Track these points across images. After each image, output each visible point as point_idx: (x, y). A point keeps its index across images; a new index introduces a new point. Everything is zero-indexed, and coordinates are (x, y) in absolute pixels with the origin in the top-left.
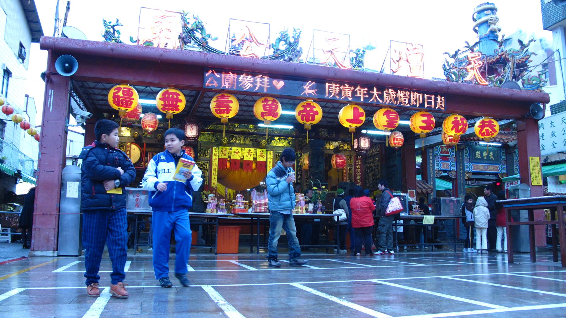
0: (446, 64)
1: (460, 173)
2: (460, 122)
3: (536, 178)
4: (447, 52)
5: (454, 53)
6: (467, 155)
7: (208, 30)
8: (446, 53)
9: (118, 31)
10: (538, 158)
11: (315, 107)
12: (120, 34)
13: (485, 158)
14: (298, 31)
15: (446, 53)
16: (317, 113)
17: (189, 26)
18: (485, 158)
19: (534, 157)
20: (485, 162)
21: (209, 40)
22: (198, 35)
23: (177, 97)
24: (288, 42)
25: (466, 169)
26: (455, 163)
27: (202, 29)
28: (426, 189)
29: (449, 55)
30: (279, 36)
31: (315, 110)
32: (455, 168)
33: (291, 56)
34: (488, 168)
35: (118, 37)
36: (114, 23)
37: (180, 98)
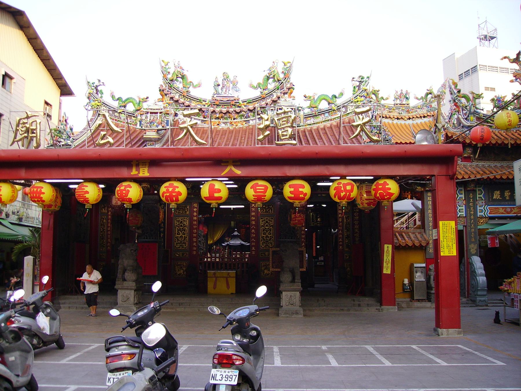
0: (453, 87)
1: (471, 220)
2: (342, 189)
3: (448, 246)
4: (507, 55)
5: (515, 57)
6: (481, 196)
7: (190, 77)
8: (505, 58)
9: (101, 91)
10: (453, 223)
11: (178, 187)
12: (102, 93)
13: (507, 198)
14: (288, 65)
15: (505, 58)
16: (180, 194)
17: (170, 76)
18: (507, 198)
19: (446, 222)
20: (507, 203)
21: (191, 89)
22: (179, 85)
23: (41, 190)
24: (276, 79)
25: (479, 214)
26: (464, 208)
27: (183, 77)
28: (420, 241)
29: (510, 60)
30: (266, 73)
31: (177, 190)
32: (464, 213)
33: (279, 94)
34: (511, 211)
35: (101, 97)
36: (97, 83)
37: (43, 190)
